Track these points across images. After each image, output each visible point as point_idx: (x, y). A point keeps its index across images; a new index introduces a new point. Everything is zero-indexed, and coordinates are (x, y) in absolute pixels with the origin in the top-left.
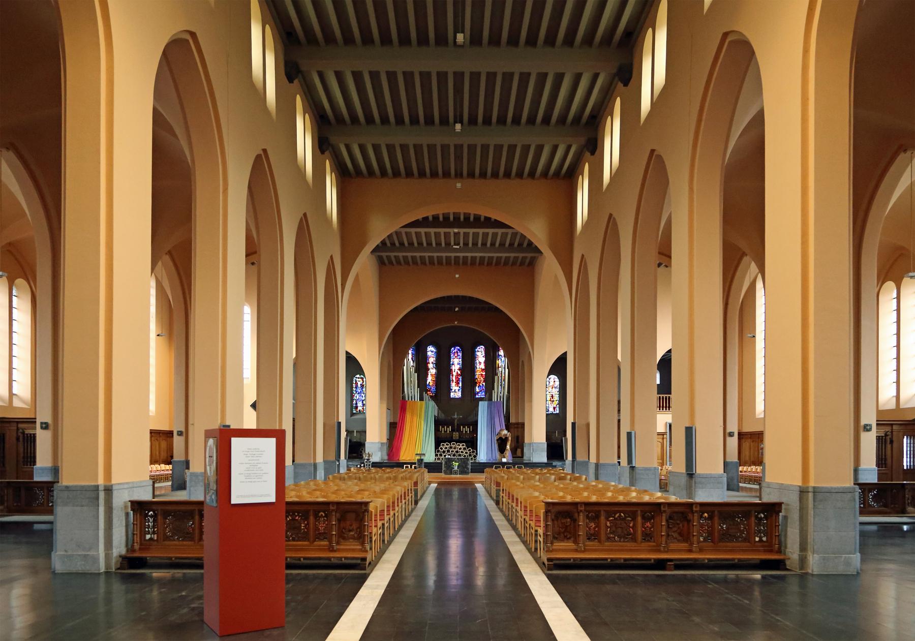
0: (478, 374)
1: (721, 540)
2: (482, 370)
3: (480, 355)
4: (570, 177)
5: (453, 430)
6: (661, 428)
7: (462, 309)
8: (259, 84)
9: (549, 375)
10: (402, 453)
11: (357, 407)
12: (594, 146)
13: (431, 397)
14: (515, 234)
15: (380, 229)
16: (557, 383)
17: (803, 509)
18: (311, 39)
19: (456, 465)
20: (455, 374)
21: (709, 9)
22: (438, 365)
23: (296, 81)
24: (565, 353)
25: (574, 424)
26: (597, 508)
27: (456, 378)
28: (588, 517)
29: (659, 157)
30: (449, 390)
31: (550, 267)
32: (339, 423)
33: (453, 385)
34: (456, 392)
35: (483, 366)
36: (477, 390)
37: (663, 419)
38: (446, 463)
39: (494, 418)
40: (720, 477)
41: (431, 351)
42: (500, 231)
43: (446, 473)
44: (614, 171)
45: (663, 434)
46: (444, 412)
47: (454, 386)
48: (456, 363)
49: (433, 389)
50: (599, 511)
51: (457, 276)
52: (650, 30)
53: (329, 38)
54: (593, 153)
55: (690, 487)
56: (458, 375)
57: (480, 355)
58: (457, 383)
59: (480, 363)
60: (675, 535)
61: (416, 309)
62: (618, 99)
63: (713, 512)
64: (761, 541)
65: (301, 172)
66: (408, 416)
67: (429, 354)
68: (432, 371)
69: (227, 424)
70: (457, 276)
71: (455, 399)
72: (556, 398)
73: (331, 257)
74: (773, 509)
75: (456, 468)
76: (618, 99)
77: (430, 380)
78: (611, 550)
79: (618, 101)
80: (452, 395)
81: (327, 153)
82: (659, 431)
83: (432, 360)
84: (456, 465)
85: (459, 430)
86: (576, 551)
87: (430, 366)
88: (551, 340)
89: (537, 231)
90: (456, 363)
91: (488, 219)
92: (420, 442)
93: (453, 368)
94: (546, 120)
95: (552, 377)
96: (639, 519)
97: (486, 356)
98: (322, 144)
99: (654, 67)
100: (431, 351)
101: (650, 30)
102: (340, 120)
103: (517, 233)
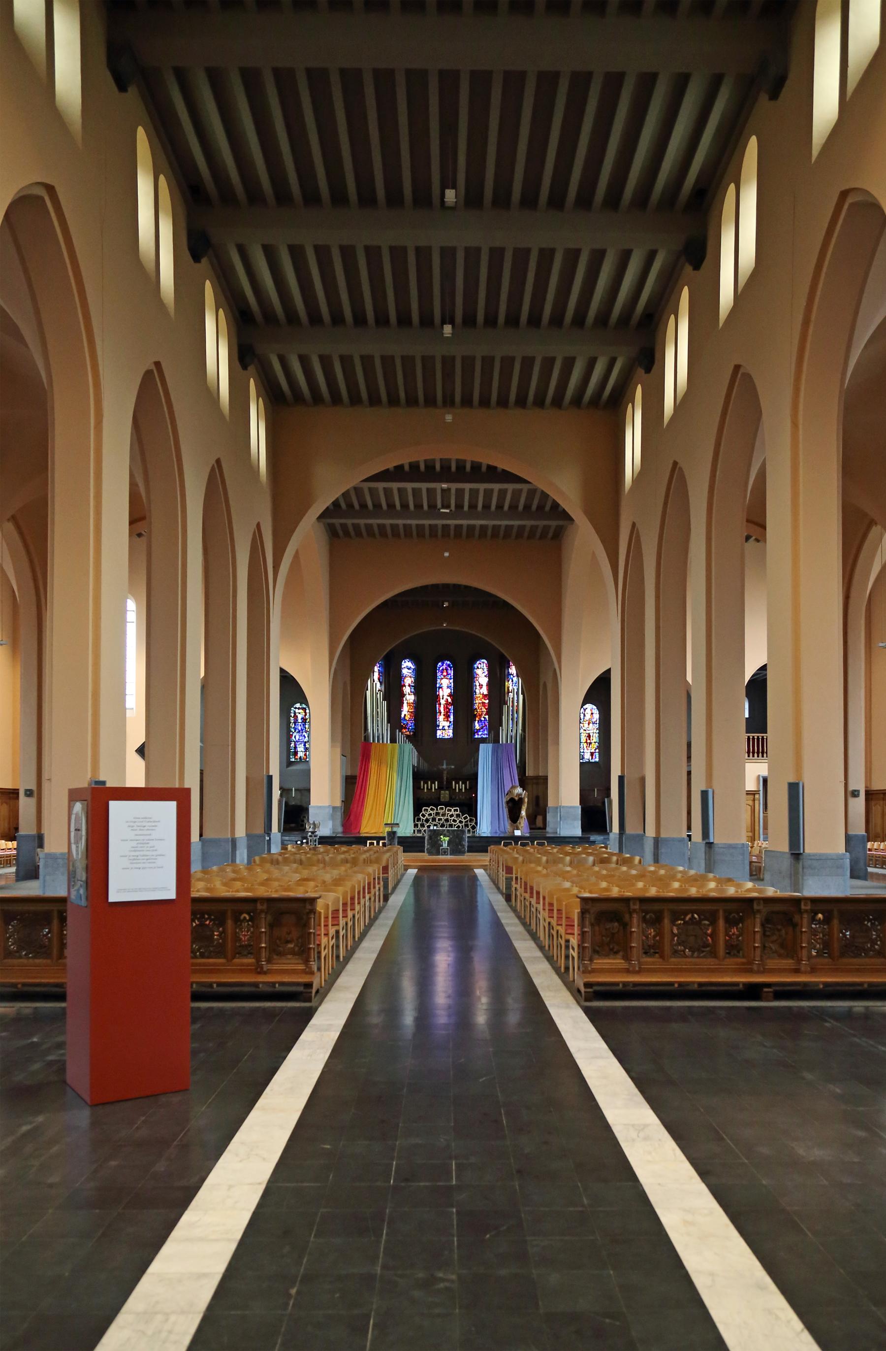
2: (484, 696)
4: (614, 406)
5: (440, 788)
7: (453, 604)
8: (150, 266)
9: (584, 704)
11: (296, 753)
12: (649, 359)
13: (408, 737)
14: (532, 492)
15: (330, 484)
19: (445, 840)
20: (443, 702)
22: (418, 689)
24: (608, 671)
25: (621, 779)
26: (656, 907)
27: (446, 708)
29: (681, 469)
30: (435, 726)
33: (441, 718)
34: (445, 729)
35: (485, 690)
36: (477, 726)
38: (430, 838)
40: (840, 857)
41: (407, 667)
42: (510, 487)
43: (430, 853)
47: (442, 722)
48: (445, 687)
49: (411, 725)
52: (673, 317)
54: (697, 266)
56: (447, 703)
58: (447, 717)
59: (481, 686)
65: (213, 396)
66: (373, 766)
67: (405, 672)
68: (410, 698)
70: (446, 554)
71: (443, 740)
72: (595, 738)
73: (258, 525)
75: (445, 845)
77: (406, 711)
79: (685, 292)
81: (252, 369)
82: (194, 894)
84: (445, 840)
85: (449, 787)
87: (407, 690)
88: (587, 651)
89: (566, 488)
90: (445, 687)
92: (392, 806)
93: (441, 693)
94: (579, 321)
95: (589, 706)
96: (721, 923)
97: (491, 675)
98: (244, 355)
99: (739, 243)
100: (407, 667)
101: (673, 317)
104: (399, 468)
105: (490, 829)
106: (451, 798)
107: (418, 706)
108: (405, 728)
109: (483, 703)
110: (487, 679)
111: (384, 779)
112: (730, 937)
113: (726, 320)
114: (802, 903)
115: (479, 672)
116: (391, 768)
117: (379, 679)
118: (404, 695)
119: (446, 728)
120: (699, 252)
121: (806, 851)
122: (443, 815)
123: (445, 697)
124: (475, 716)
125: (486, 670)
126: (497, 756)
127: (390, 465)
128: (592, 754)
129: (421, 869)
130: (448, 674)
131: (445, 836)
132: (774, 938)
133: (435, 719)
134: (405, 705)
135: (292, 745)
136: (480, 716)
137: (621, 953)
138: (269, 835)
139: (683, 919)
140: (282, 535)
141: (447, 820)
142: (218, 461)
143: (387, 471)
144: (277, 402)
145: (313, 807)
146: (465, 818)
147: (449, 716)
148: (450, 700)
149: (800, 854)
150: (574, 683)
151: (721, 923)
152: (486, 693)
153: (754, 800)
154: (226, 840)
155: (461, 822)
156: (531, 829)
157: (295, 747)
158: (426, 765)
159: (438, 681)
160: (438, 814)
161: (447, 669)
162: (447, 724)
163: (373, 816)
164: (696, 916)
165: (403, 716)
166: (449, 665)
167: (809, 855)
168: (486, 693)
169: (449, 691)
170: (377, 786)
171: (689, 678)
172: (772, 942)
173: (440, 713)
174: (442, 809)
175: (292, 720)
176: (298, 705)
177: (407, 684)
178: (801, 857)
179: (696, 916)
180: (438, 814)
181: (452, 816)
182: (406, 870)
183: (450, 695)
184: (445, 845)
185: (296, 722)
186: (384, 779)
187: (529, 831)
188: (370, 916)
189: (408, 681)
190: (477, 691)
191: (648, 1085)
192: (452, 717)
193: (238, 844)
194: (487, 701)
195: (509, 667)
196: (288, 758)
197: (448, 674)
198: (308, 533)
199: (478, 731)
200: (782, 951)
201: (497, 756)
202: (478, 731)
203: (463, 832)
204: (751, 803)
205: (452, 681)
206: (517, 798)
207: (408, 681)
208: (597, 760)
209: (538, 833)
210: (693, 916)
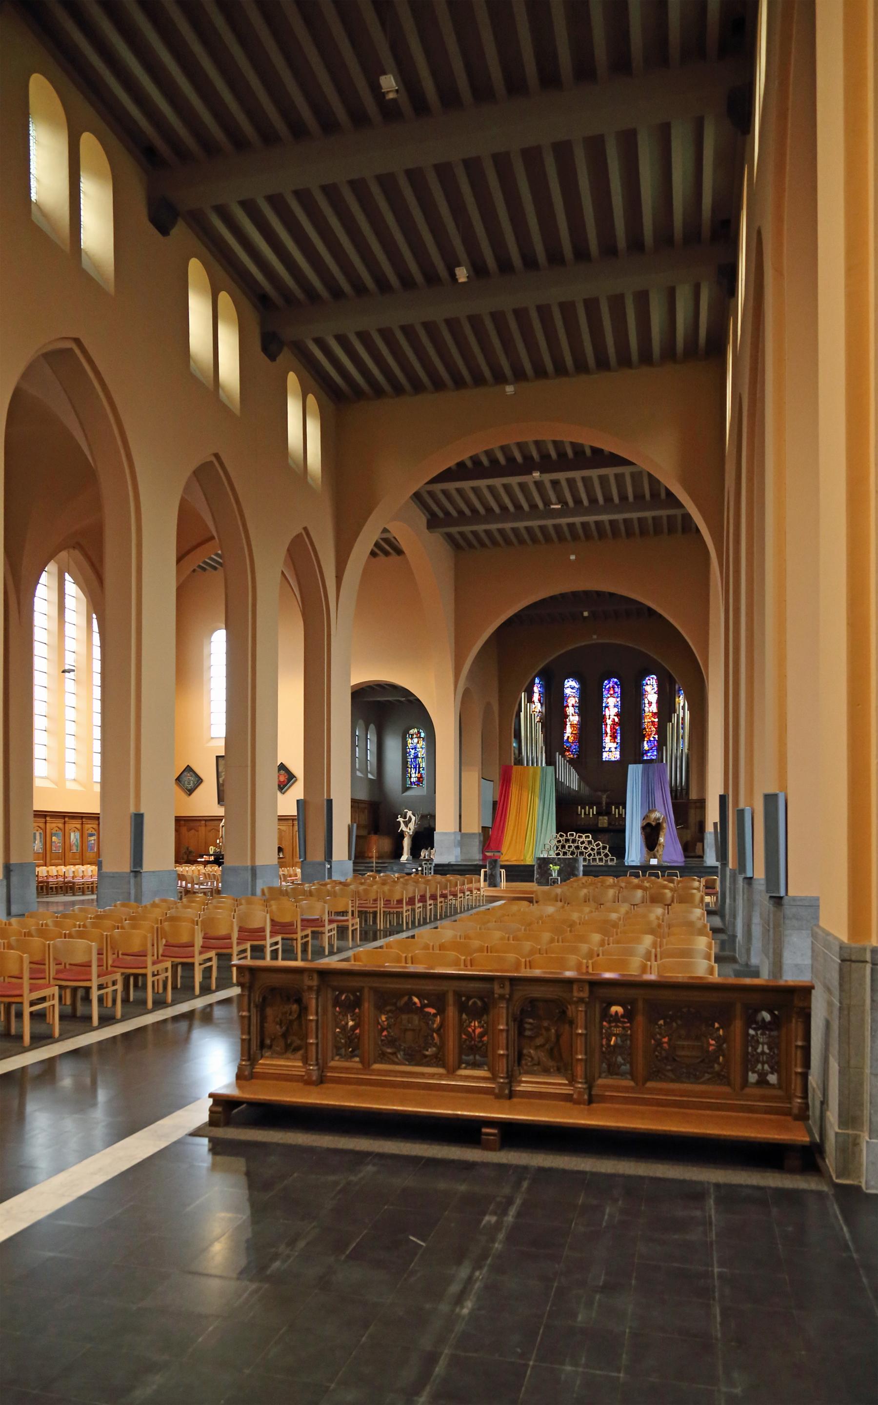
1: (655, 1074)
2: (654, 714)
5: (599, 813)
7: (593, 614)
10: (504, 849)
13: (571, 762)
14: (637, 477)
17: (846, 1010)
18: (182, 153)
19: (555, 869)
20: (609, 722)
22: (582, 709)
23: (174, 232)
26: (355, 983)
28: (337, 1002)
30: (601, 748)
33: (607, 739)
34: (611, 751)
35: (654, 708)
36: (646, 747)
38: (540, 867)
39: (653, 793)
41: (571, 686)
42: (610, 472)
43: (540, 883)
46: (587, 783)
47: (609, 743)
48: (612, 707)
49: (575, 747)
50: (361, 990)
51: (573, 557)
53: (210, 148)
55: (777, 926)
58: (614, 737)
59: (650, 703)
60: (542, 1055)
61: (517, 616)
63: (633, 1002)
64: (762, 1081)
66: (514, 790)
67: (568, 691)
68: (574, 719)
70: (573, 557)
71: (609, 762)
74: (791, 1002)
75: (555, 875)
82: (281, 812)
84: (555, 869)
85: (608, 813)
86: (307, 1082)
87: (570, 710)
90: (612, 707)
91: (596, 451)
92: (535, 834)
93: (607, 713)
96: (451, 1012)
97: (659, 693)
100: (571, 686)
102: (288, 297)
103: (641, 473)
104: (461, 465)
105: (639, 856)
106: (609, 824)
108: (569, 751)
109: (653, 722)
110: (656, 696)
111: (525, 804)
112: (469, 1035)
114: (575, 987)
115: (648, 688)
116: (533, 792)
117: (539, 700)
118: (567, 716)
119: (613, 749)
121: (790, 894)
122: (574, 841)
123: (612, 717)
124: (644, 736)
125: (655, 686)
126: (648, 778)
127: (451, 463)
130: (615, 692)
131: (556, 865)
132: (539, 1041)
133: (601, 741)
134: (568, 727)
136: (650, 735)
137: (301, 1052)
138: (330, 863)
139: (395, 1004)
141: (577, 848)
143: (449, 470)
144: (338, 402)
145: (439, 833)
146: (598, 845)
147: (616, 737)
148: (617, 720)
149: (781, 898)
151: (451, 1012)
152: (655, 710)
154: (245, 868)
155: (592, 849)
156: (686, 857)
158: (587, 788)
159: (605, 700)
160: (567, 841)
161: (613, 687)
162: (615, 745)
163: (514, 842)
164: (416, 1000)
165: (565, 738)
166: (616, 683)
167: (794, 899)
168: (655, 710)
169: (616, 710)
170: (519, 811)
172: (537, 1048)
173: (607, 733)
174: (572, 835)
177: (570, 705)
178: (786, 901)
179: (416, 1000)
180: (567, 841)
181: (583, 843)
183: (617, 715)
184: (555, 875)
186: (525, 804)
187: (683, 859)
189: (572, 701)
190: (646, 709)
192: (619, 738)
193: (258, 872)
194: (656, 720)
197: (615, 692)
199: (648, 751)
200: (551, 1063)
201: (648, 778)
202: (648, 751)
203: (576, 860)
205: (619, 699)
206: (654, 824)
207: (572, 701)
209: (694, 862)
210: (410, 999)
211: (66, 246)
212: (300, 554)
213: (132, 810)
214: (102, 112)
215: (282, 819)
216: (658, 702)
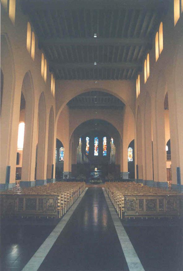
0: (104, 147)
2: (106, 146)
3: (105, 139)
4: (135, 79)
6: (168, 167)
8: (29, 50)
9: (128, 148)
11: (61, 159)
15: (69, 97)
16: (132, 150)
20: (96, 147)
21: (146, 82)
22: (89, 144)
24: (134, 140)
25: (137, 166)
27: (96, 148)
30: (94, 153)
31: (128, 110)
32: (9, 168)
35: (106, 144)
37: (168, 164)
41: (87, 139)
44: (160, 52)
45: (169, 169)
48: (96, 143)
52: (157, 33)
56: (97, 147)
57: (105, 139)
58: (97, 150)
62: (139, 75)
65: (42, 78)
68: (88, 146)
69: (10, 166)
70: (96, 113)
72: (132, 155)
73: (52, 106)
76: (139, 75)
77: (87, 149)
78: (53, 114)
80: (95, 154)
82: (167, 168)
83: (88, 142)
87: (87, 144)
88: (129, 135)
89: (124, 96)
90: (96, 143)
93: (95, 145)
95: (130, 148)
97: (107, 141)
100: (87, 139)
101: (157, 33)
107: (90, 148)
113: (176, 24)
118: (86, 145)
120: (151, 47)
128: (131, 159)
129: (89, 188)
133: (94, 151)
135: (60, 157)
140: (58, 108)
142: (43, 92)
144: (57, 79)
148: (97, 146)
150: (126, 141)
153: (170, 170)
157: (61, 158)
169: (97, 144)
171: (152, 140)
175: (60, 151)
176: (62, 148)
182: (86, 188)
183: (98, 145)
185: (61, 152)
188: (63, 213)
191: (57, 128)
194: (106, 147)
195: (111, 139)
196: (59, 160)
198: (64, 106)
204: (169, 171)
208: (132, 161)
211: (30, 52)
212: (52, 110)
213: (7, 165)
214: (37, 31)
215: (167, 169)
216: (107, 143)
